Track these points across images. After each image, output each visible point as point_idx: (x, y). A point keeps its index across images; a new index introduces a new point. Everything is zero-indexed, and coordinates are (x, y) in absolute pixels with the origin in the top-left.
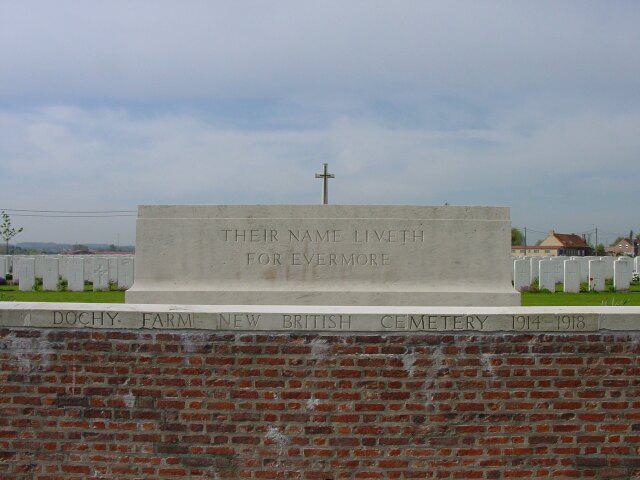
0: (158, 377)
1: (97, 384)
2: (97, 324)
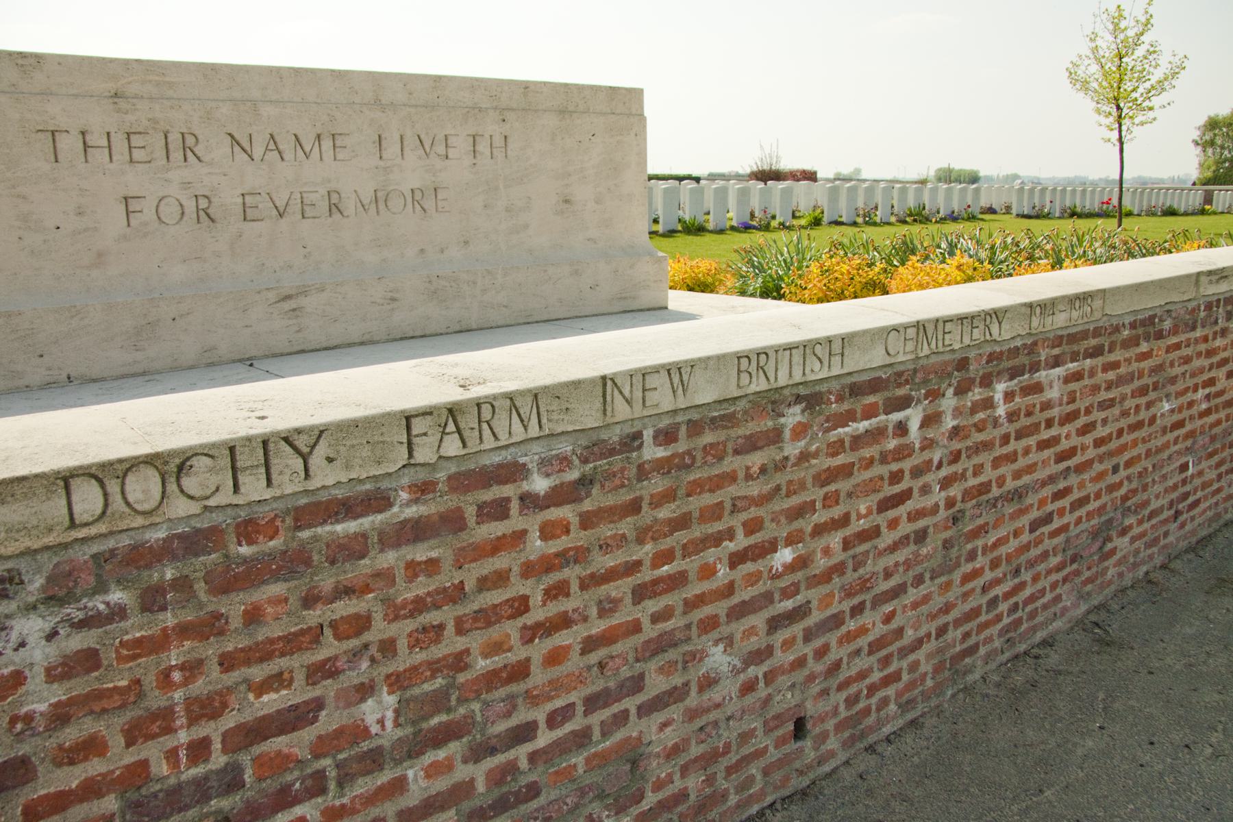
0: (460, 610)
1: (272, 701)
2: (254, 488)
